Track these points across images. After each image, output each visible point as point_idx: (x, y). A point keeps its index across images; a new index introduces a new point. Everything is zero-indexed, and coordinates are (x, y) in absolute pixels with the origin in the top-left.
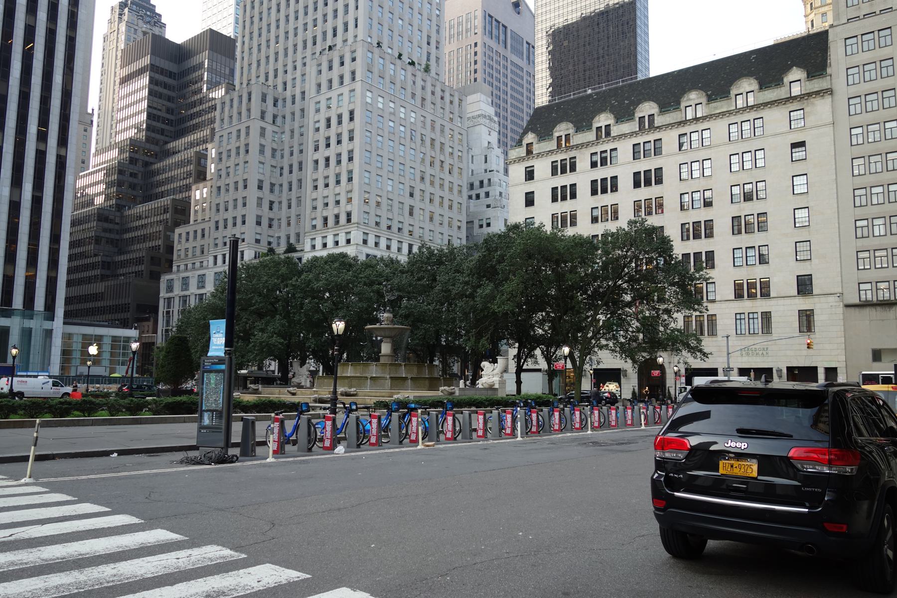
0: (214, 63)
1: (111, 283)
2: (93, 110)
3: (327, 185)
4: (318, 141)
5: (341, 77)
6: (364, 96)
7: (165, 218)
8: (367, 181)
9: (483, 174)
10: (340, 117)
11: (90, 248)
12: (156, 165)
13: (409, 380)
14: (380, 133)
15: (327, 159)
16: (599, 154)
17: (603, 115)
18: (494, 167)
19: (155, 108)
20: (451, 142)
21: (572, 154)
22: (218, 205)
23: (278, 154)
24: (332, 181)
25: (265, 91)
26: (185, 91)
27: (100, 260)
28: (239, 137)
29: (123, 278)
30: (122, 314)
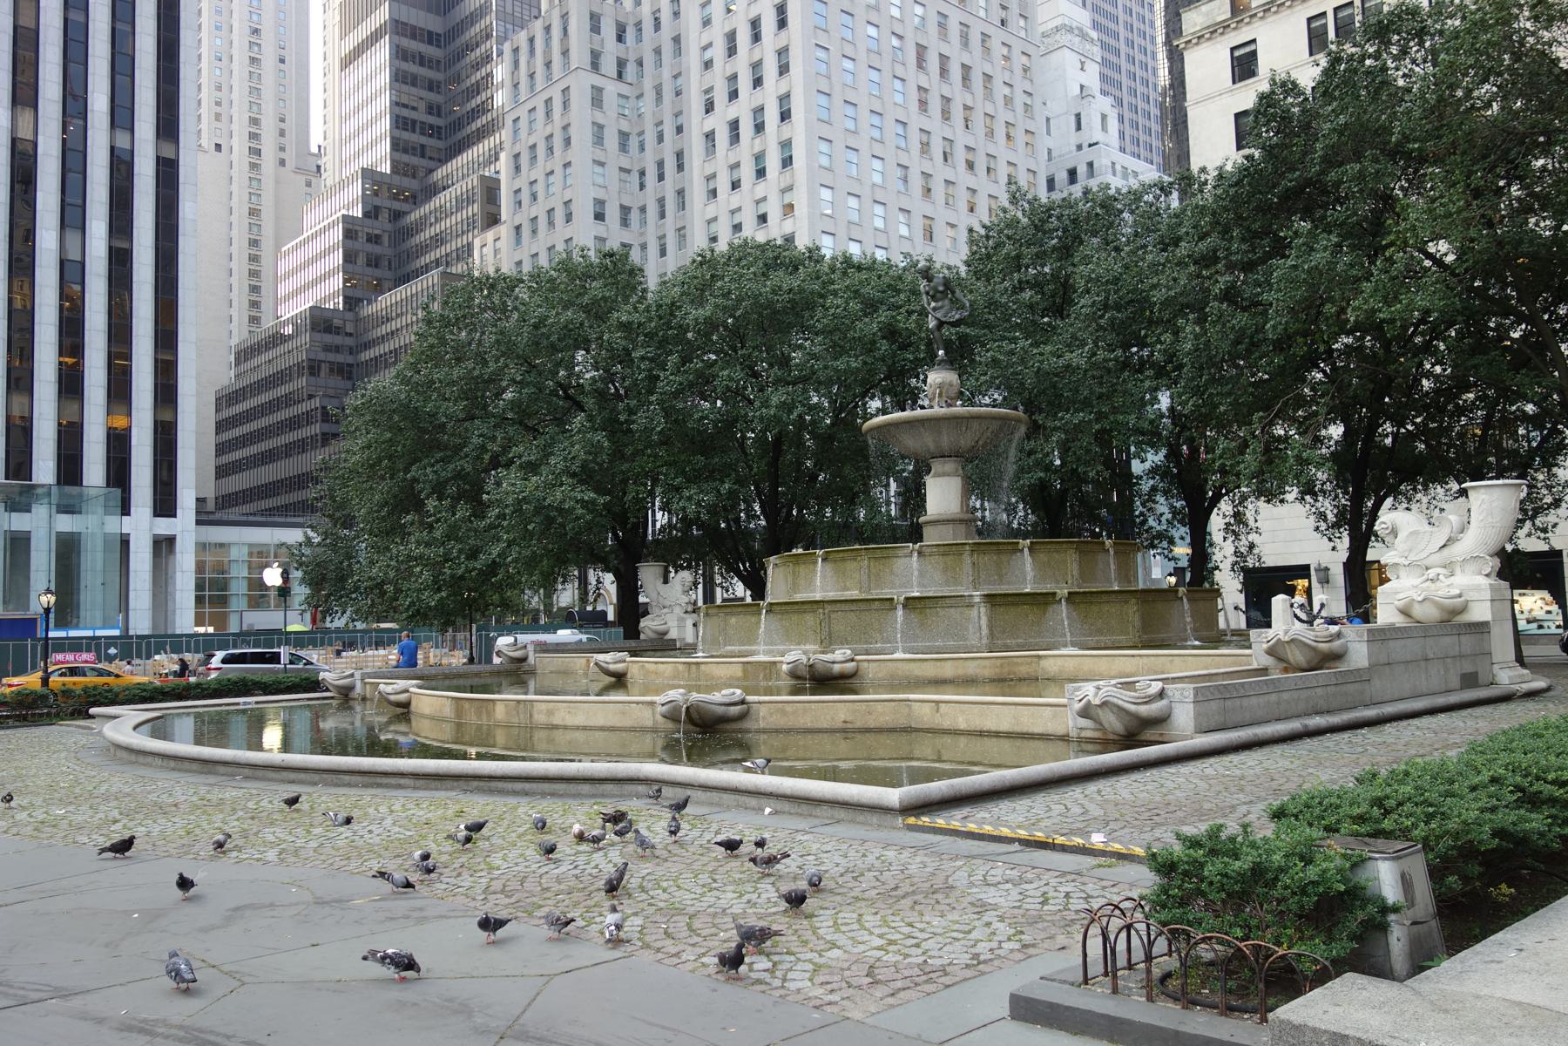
3: (735, 185)
8: (825, 161)
9: (1075, 153)
10: (755, 24)
11: (301, 382)
13: (900, 612)
14: (849, 51)
18: (1097, 136)
19: (405, 106)
20: (1007, 74)
23: (633, 143)
25: (596, 9)
26: (458, 66)
28: (548, 113)
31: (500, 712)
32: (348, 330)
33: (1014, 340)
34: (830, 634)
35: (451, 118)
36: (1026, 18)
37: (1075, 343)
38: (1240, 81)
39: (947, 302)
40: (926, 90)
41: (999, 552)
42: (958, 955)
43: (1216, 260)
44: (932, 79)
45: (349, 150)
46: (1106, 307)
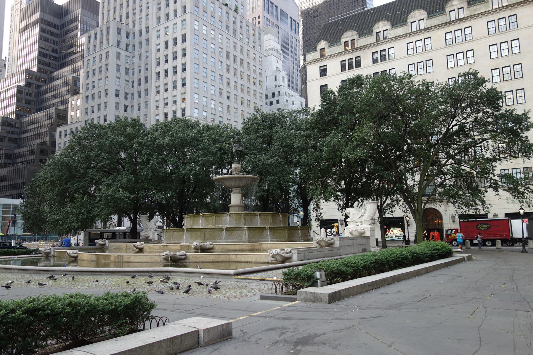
0: (85, 18)
1: (12, 168)
2: (6, 58)
3: (166, 90)
4: (159, 58)
5: (176, 11)
6: (192, 24)
7: (50, 122)
8: (196, 86)
10: (175, 39)
12: (45, 87)
13: (268, 232)
14: (205, 52)
15: (166, 71)
16: (379, 52)
17: (381, 23)
18: (281, 83)
19: (44, 49)
20: (254, 63)
21: (357, 54)
22: (87, 109)
23: (130, 72)
24: (170, 87)
26: (65, 37)
27: (3, 152)
28: (101, 60)
29: (20, 164)
30: (20, 190)
31: (112, 258)
32: (17, 126)
33: (256, 155)
34: (204, 237)
35: (62, 54)
36: (261, 46)
37: (273, 156)
38: (322, 76)
39: (238, 144)
40: (229, 66)
41: (251, 215)
42: (250, 294)
43: (311, 137)
44: (231, 62)
45: (20, 62)
46: (282, 146)
